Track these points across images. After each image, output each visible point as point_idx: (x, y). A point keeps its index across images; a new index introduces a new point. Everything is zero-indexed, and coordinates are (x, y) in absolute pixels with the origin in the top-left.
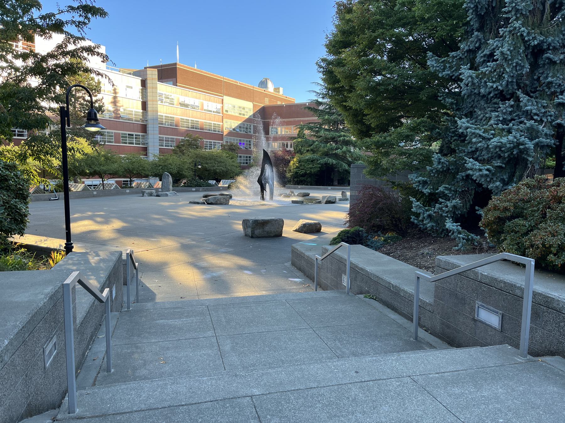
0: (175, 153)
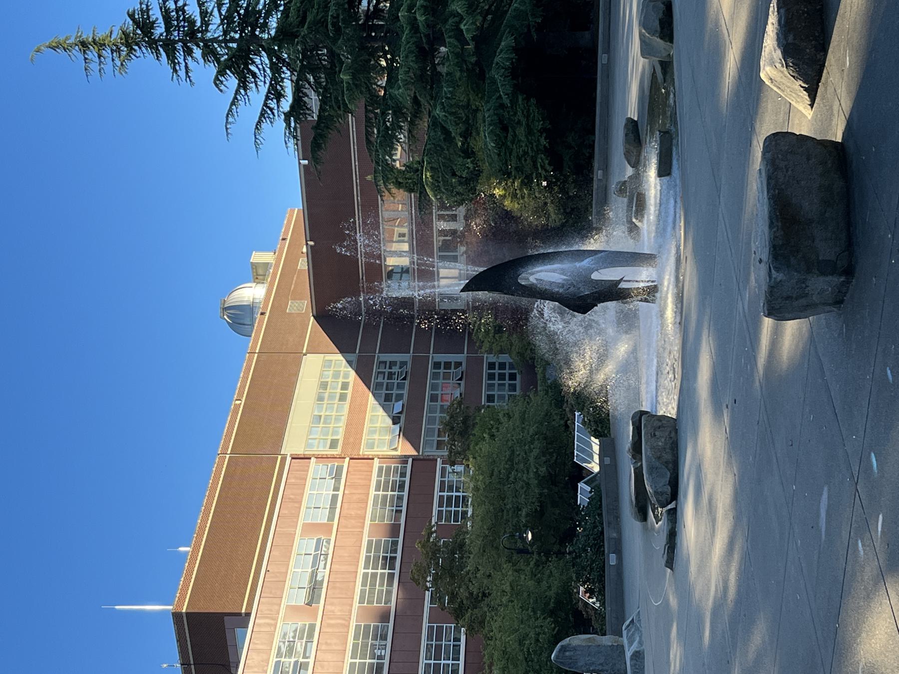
0: (482, 623)
